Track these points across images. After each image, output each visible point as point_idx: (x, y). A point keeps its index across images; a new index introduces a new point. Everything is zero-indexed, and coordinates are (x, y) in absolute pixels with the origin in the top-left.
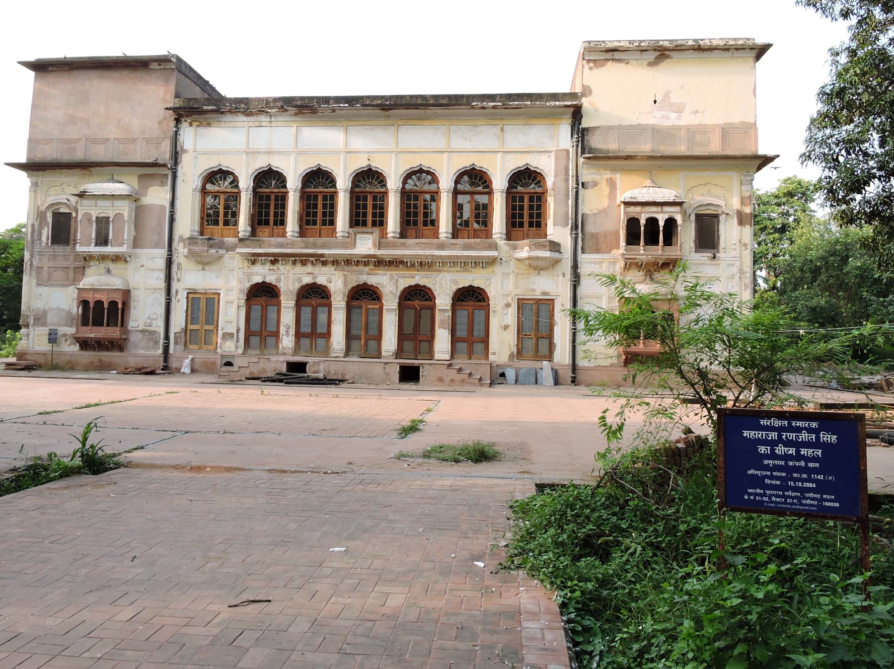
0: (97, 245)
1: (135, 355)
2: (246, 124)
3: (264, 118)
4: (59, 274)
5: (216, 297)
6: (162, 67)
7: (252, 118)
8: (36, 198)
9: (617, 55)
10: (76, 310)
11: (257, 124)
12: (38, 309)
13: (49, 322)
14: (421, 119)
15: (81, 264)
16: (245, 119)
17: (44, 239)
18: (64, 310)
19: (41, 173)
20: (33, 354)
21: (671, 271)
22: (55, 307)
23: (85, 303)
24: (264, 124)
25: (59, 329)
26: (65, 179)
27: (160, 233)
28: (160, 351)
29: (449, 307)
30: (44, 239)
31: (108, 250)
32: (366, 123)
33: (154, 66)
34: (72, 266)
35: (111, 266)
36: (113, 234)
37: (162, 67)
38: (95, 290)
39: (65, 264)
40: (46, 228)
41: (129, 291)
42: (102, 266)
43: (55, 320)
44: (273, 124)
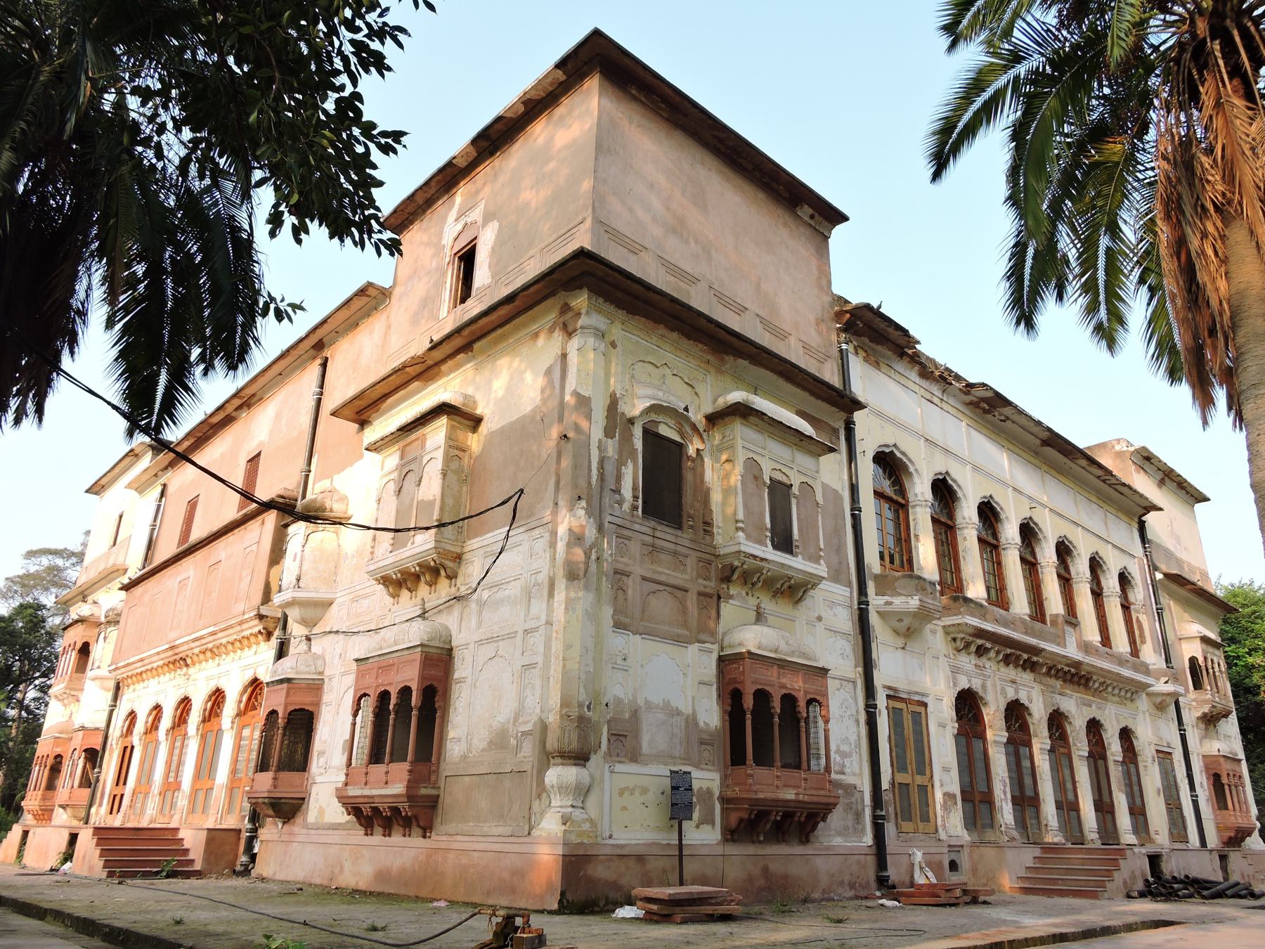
0: (775, 547)
1: (830, 853)
2: (917, 388)
3: (936, 389)
4: (662, 605)
5: (922, 709)
6: (812, 222)
7: (925, 384)
8: (607, 375)
9: (1147, 465)
10: (711, 715)
11: (928, 396)
12: (619, 701)
13: (645, 748)
14: (1058, 472)
15: (711, 585)
16: (918, 380)
17: (627, 492)
18: (679, 713)
19: (621, 314)
20: (611, 857)
21: (741, 682)
22: (656, 699)
23: (732, 698)
24: (936, 400)
25: (695, 774)
26: (670, 357)
27: (840, 549)
28: (868, 839)
29: (714, 680)
30: (627, 492)
31: (797, 563)
32: (1022, 453)
33: (805, 211)
34: (694, 589)
35: (768, 605)
36: (800, 529)
37: (812, 222)
38: (783, 664)
39: (679, 578)
40: (630, 465)
41: (451, 649)
42: (752, 602)
43: (662, 743)
44: (945, 406)
